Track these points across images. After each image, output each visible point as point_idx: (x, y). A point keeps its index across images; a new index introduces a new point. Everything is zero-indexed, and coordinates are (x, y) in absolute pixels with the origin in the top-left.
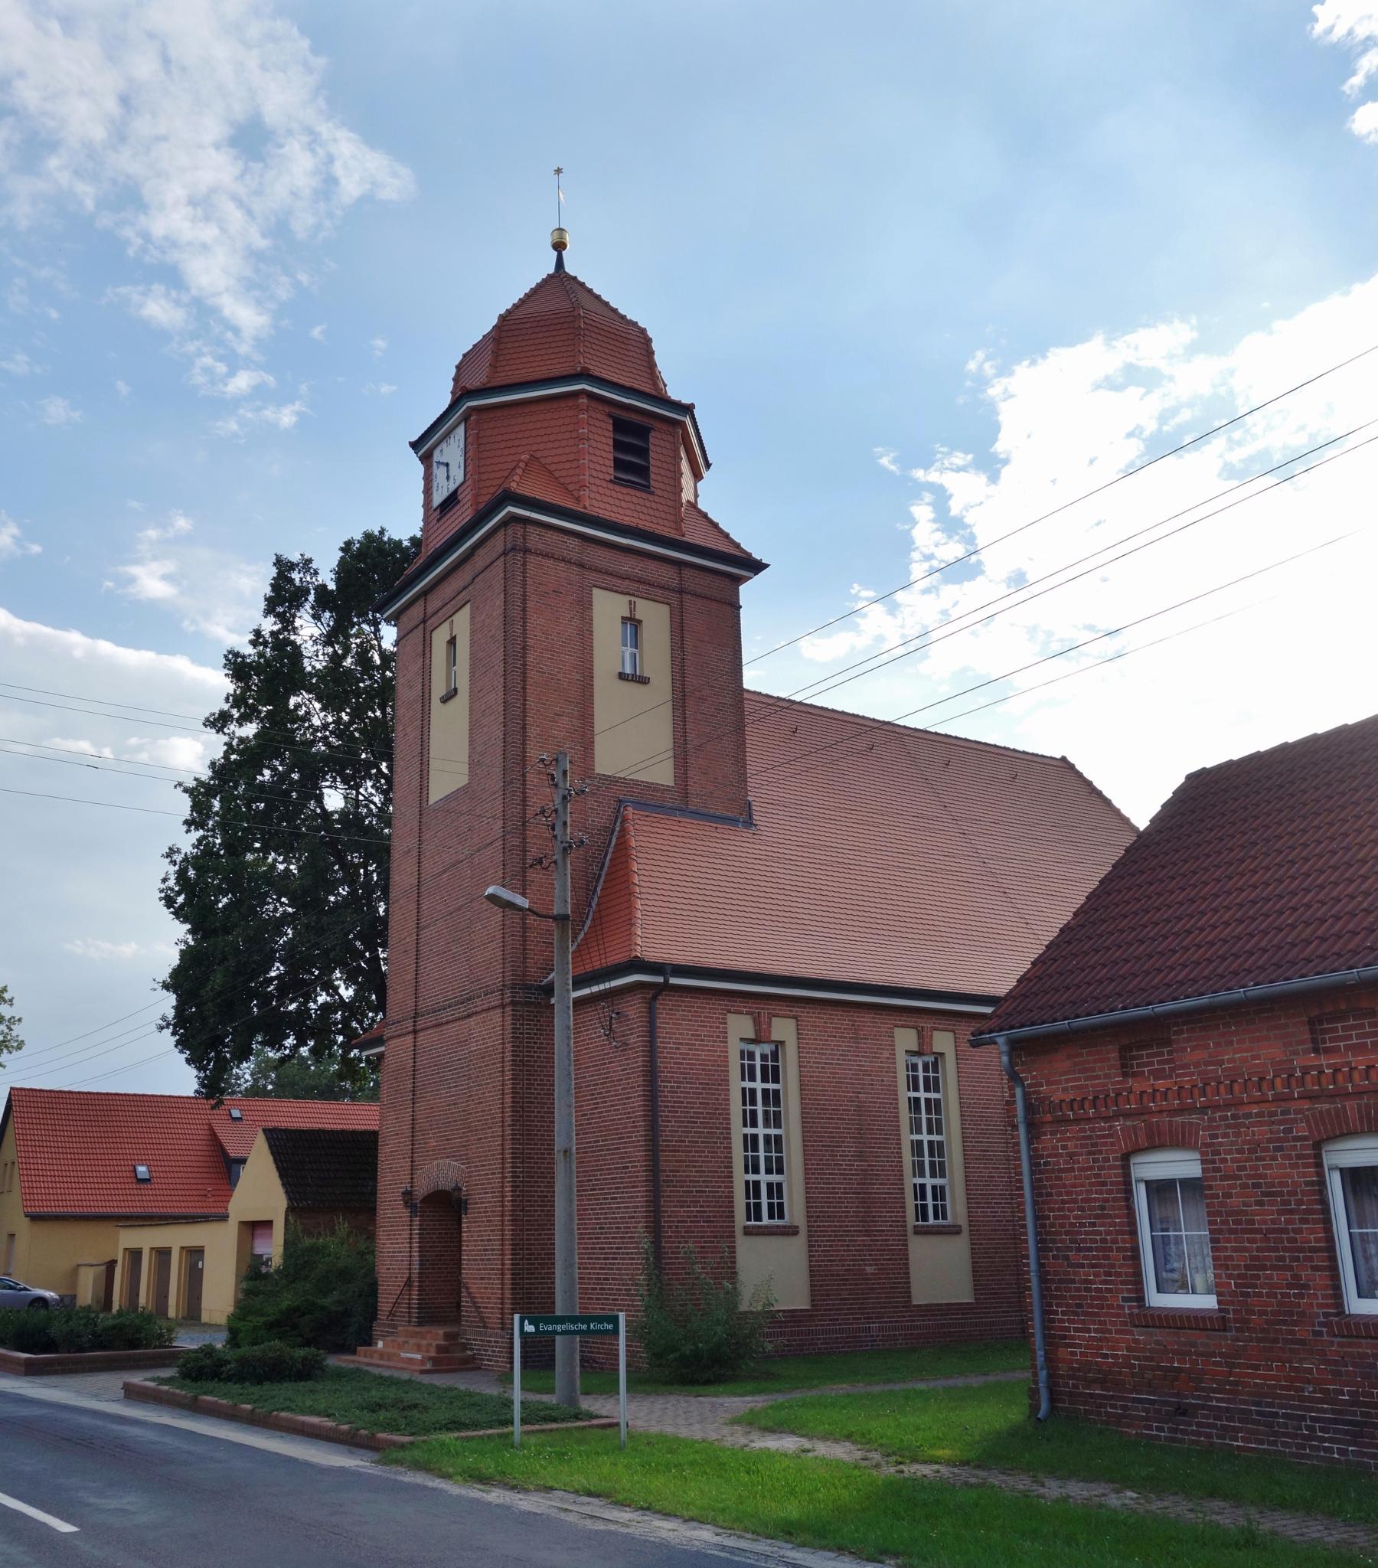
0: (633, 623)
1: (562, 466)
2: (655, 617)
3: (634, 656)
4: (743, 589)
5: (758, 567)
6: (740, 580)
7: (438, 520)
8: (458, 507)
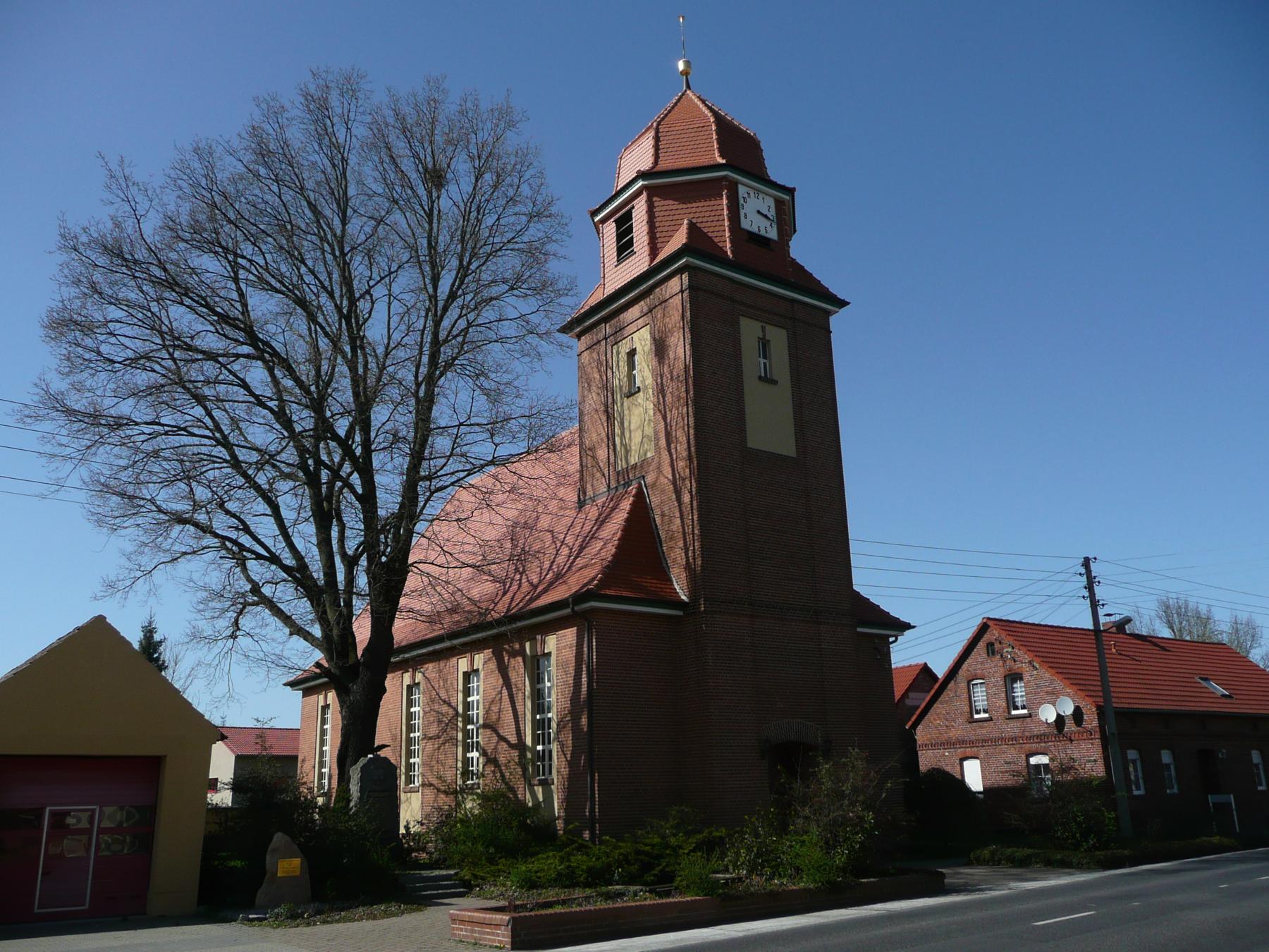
0: (764, 344)
1: (709, 224)
2: (778, 338)
3: (765, 364)
4: (833, 319)
5: (842, 304)
6: (828, 313)
7: (616, 266)
8: (634, 256)
